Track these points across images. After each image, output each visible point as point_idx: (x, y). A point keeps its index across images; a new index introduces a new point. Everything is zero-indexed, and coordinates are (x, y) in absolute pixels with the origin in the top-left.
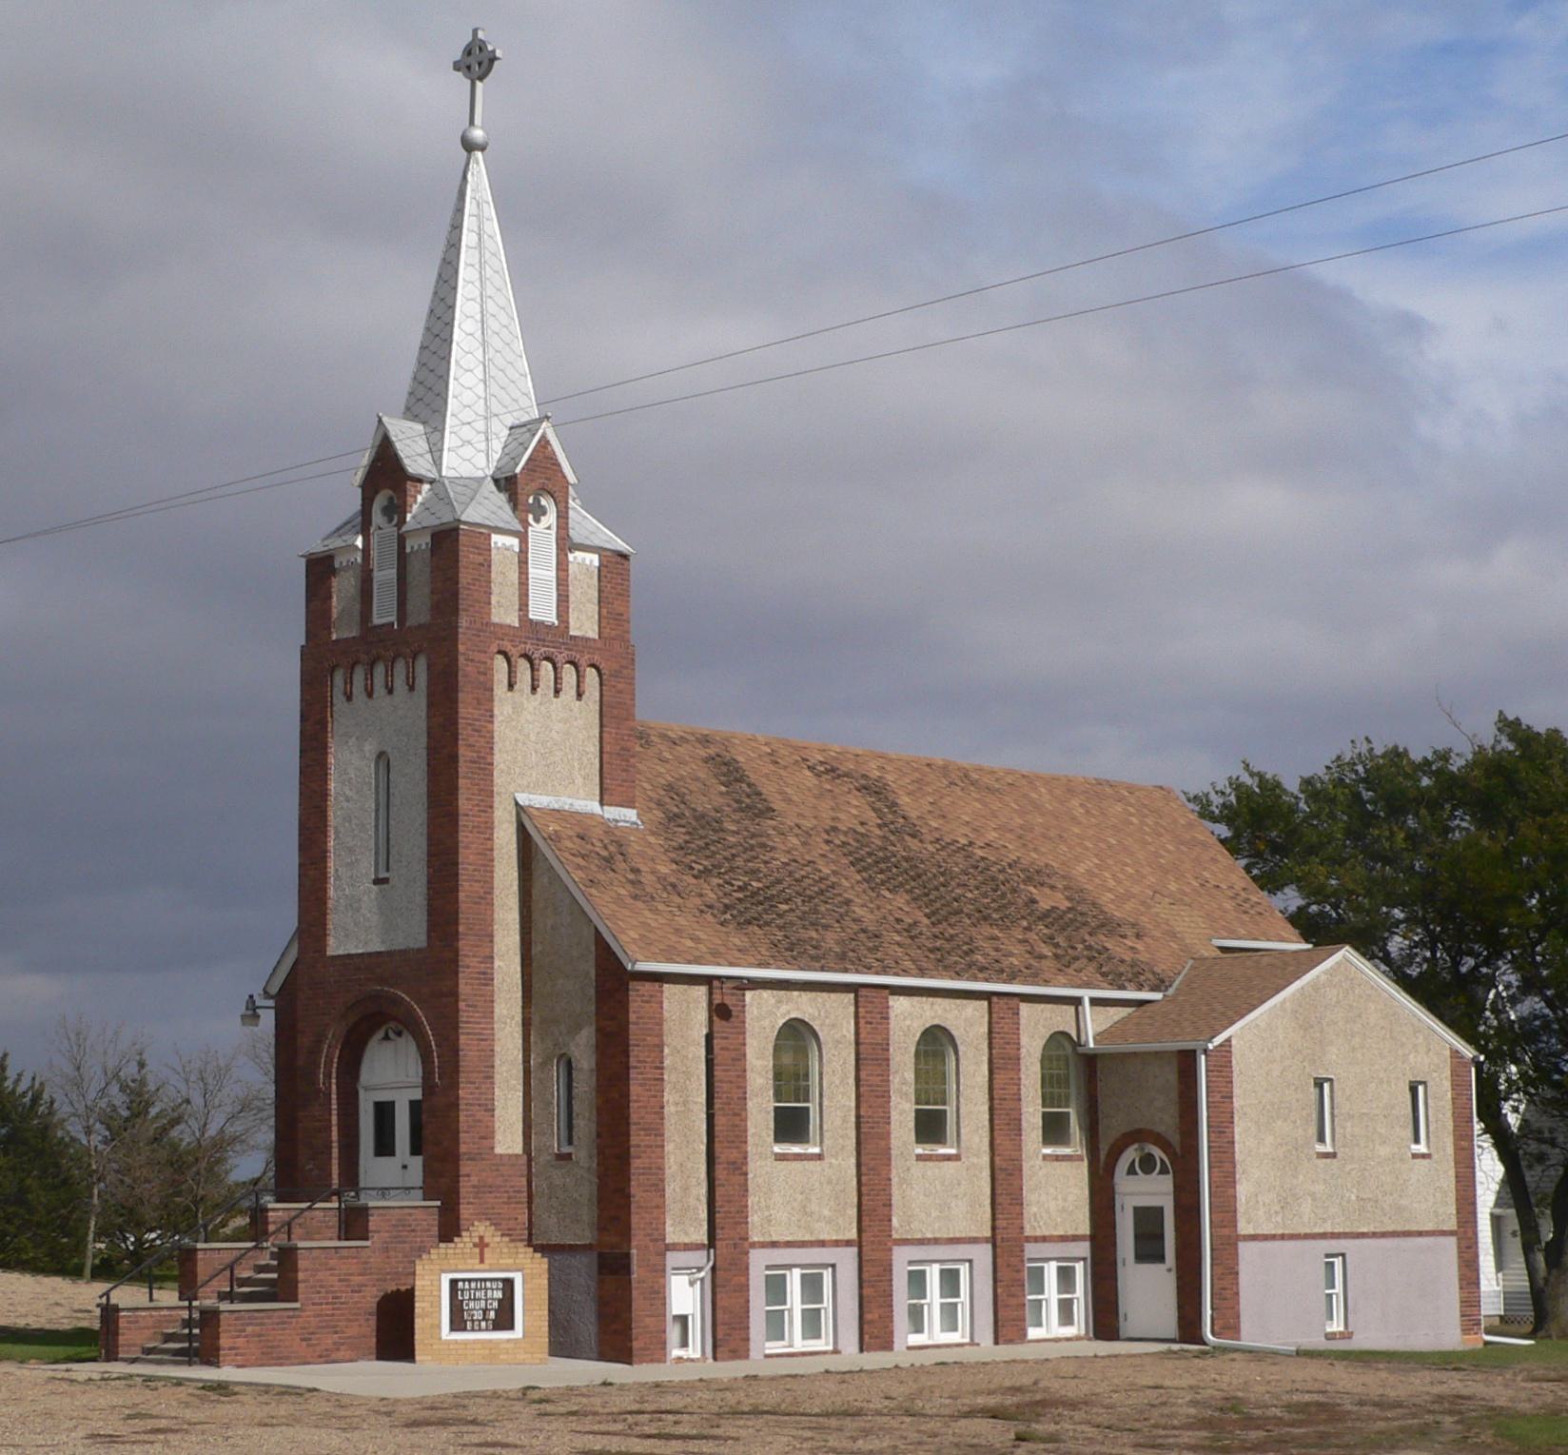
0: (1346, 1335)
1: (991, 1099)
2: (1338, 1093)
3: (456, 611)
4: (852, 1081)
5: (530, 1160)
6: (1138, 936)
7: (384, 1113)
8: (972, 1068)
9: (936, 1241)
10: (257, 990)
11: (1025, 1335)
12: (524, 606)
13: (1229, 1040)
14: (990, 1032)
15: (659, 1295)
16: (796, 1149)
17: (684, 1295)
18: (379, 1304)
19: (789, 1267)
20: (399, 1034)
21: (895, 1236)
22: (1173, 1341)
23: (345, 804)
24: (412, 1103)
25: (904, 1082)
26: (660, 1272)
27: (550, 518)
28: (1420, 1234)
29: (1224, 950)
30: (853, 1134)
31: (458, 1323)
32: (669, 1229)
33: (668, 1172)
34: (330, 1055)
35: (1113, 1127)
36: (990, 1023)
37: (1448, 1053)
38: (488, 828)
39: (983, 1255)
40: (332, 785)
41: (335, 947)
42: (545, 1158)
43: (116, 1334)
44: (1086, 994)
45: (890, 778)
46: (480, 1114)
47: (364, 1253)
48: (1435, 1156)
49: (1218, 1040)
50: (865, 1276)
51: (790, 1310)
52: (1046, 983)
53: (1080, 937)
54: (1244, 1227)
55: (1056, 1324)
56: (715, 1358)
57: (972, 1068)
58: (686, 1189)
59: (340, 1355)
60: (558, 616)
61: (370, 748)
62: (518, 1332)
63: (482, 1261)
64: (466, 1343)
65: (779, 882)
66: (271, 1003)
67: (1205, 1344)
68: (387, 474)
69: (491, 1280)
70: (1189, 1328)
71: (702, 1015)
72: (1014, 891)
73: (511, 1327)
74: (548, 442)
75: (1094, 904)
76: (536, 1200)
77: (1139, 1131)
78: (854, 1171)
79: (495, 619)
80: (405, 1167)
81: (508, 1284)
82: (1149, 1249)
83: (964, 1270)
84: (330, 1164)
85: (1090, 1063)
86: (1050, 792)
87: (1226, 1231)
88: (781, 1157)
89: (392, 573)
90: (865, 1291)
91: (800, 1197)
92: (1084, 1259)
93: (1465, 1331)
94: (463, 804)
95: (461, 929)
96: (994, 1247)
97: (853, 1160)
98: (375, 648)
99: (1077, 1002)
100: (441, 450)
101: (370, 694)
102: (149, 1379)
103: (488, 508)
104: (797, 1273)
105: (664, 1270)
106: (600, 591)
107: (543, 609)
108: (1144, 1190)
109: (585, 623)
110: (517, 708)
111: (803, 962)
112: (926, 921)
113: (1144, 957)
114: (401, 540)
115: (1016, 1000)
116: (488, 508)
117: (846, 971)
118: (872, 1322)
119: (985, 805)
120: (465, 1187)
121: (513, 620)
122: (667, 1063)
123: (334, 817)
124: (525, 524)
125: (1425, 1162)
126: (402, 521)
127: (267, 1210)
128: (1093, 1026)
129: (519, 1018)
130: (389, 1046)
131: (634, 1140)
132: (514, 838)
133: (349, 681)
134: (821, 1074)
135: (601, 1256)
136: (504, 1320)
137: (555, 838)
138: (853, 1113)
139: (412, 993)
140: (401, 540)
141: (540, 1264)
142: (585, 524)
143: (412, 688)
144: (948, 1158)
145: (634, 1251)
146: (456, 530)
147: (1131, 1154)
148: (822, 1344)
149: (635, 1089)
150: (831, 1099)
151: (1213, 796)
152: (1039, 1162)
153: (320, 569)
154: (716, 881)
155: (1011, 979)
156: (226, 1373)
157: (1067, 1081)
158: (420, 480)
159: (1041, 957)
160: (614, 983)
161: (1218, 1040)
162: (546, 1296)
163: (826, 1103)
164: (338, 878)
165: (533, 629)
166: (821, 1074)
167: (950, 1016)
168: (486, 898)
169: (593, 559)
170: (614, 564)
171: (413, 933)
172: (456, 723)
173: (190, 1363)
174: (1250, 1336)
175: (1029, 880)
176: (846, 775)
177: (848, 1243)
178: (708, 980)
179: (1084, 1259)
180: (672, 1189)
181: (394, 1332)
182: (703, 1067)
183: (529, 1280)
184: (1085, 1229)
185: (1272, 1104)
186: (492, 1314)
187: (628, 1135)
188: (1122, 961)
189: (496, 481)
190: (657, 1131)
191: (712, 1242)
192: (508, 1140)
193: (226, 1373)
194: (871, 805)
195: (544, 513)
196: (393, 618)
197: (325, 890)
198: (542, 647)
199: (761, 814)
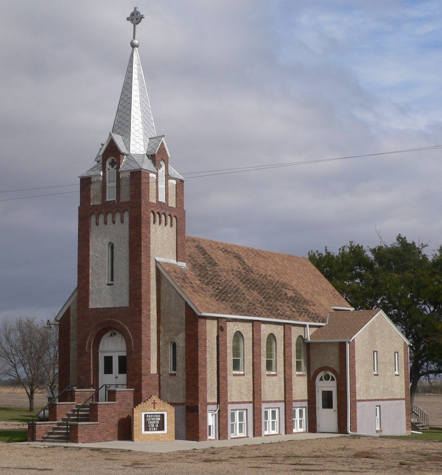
0: (381, 431)
1: (284, 356)
2: (378, 356)
3: (140, 197)
4: (251, 351)
5: (160, 375)
6: (314, 305)
7: (108, 361)
8: (280, 347)
9: (271, 402)
10: (52, 320)
11: (293, 431)
12: (157, 197)
13: (354, 339)
14: (284, 335)
15: (205, 419)
16: (237, 373)
17: (211, 420)
18: (119, 422)
19: (236, 410)
20: (115, 334)
21: (262, 400)
22: (336, 433)
23: (96, 259)
24: (120, 358)
25: (264, 352)
26: (205, 412)
27: (163, 168)
28: (397, 399)
29: (334, 310)
30: (251, 367)
31: (147, 429)
32: (208, 398)
33: (207, 380)
34: (91, 339)
35: (316, 365)
36: (284, 332)
37: (403, 343)
38: (149, 268)
39: (282, 405)
40: (91, 253)
41: (92, 305)
42: (166, 375)
43: (35, 432)
44: (308, 324)
45: (240, 253)
46: (147, 361)
47: (115, 406)
48: (400, 375)
49: (352, 339)
50: (255, 412)
51: (236, 424)
52: (298, 320)
53: (300, 306)
54: (358, 398)
55: (300, 427)
56: (219, 439)
57: (280, 347)
58: (212, 385)
59: (108, 439)
60: (166, 200)
61: (107, 241)
62: (165, 431)
63: (154, 408)
64: (149, 435)
65: (226, 287)
66: (57, 323)
67: (348, 434)
68: (112, 153)
69: (157, 414)
70: (342, 428)
71: (215, 330)
72: (281, 291)
73: (163, 429)
74: (163, 144)
75: (300, 295)
76: (162, 389)
77: (325, 367)
78: (252, 379)
79: (150, 201)
80: (117, 377)
81: (162, 416)
82: (327, 404)
83: (277, 410)
84: (90, 376)
85: (308, 345)
86: (279, 258)
87: (354, 399)
88: (235, 375)
89: (114, 184)
90: (256, 418)
91: (239, 388)
92: (306, 407)
94: (143, 261)
95: (142, 301)
96: (285, 403)
97: (252, 376)
98: (108, 208)
99: (305, 326)
100: (129, 145)
101: (106, 223)
102: (65, 447)
103: (147, 165)
104: (238, 411)
105: (206, 411)
106: (176, 192)
107: (162, 199)
108: (325, 385)
109: (172, 203)
110: (156, 230)
111: (240, 313)
112: (264, 300)
113: (317, 312)
114: (118, 174)
115: (290, 325)
116: (147, 165)
117: (251, 316)
118: (257, 427)
119: (265, 262)
120: (143, 384)
121: (154, 201)
122: (207, 345)
123: (92, 263)
124: (158, 171)
126: (118, 168)
127: (75, 391)
128: (309, 333)
129: (156, 330)
131: (199, 369)
132: (155, 272)
133: (97, 219)
134: (244, 349)
135: (187, 407)
136: (161, 427)
137: (168, 272)
138: (252, 361)
139: (126, 321)
140: (118, 174)
141: (172, 409)
142: (173, 171)
143: (122, 222)
144: (274, 375)
145: (199, 405)
146: (141, 171)
147: (322, 374)
148: (243, 435)
149: (200, 353)
150: (372, 362)
151: (316, 255)
152: (295, 376)
153: (86, 182)
154: (211, 286)
155: (289, 319)
156: (80, 445)
157: (301, 350)
158: (123, 155)
159: (294, 312)
160: (193, 320)
161: (352, 339)
162: (174, 420)
163: (245, 358)
164: (93, 283)
166: (244, 349)
167: (275, 330)
168: (148, 291)
169: (174, 182)
170: (180, 183)
171: (123, 301)
172: (141, 234)
173: (67, 442)
174: (360, 431)
175: (283, 287)
176: (230, 252)
177: (250, 402)
178: (217, 319)
179: (306, 407)
180: (209, 385)
181: (126, 431)
182: (216, 346)
183: (169, 414)
184: (306, 397)
185: (364, 359)
186: (157, 425)
187: (198, 368)
188: (313, 313)
189: (148, 156)
190: (205, 367)
191: (218, 403)
192: (154, 370)
193: (80, 445)
194: (239, 262)
195: (161, 167)
196: (115, 199)
197: (88, 287)
198: (162, 211)
199: (214, 265)
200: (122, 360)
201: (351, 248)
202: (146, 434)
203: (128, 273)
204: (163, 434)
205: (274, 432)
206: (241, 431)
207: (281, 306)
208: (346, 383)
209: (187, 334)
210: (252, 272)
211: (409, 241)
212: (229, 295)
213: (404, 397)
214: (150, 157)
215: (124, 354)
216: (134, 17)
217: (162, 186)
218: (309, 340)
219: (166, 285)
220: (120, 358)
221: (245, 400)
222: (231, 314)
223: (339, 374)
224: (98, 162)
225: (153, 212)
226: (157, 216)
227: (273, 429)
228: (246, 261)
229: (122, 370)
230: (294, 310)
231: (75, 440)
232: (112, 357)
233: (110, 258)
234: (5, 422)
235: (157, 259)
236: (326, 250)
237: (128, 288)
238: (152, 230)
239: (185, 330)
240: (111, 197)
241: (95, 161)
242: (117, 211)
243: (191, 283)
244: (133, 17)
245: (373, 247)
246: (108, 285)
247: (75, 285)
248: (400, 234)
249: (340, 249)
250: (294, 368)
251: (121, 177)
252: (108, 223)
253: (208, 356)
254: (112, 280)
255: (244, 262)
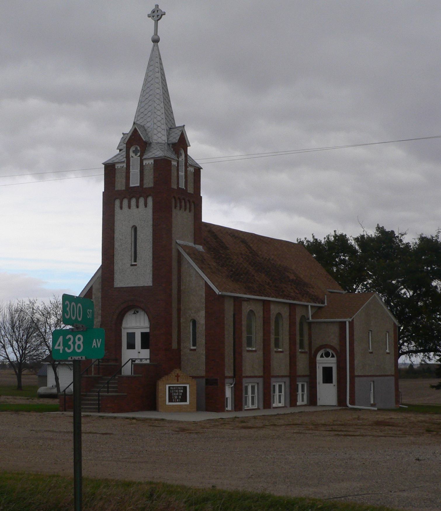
7: (131, 336)
12: (178, 184)
17: (228, 393)
20: (138, 312)
24: (143, 334)
28: (388, 376)
29: (329, 292)
31: (170, 400)
44: (310, 304)
52: (301, 301)
54: (356, 374)
60: (185, 186)
62: (188, 403)
63: (178, 381)
64: (173, 406)
77: (326, 345)
80: (139, 352)
81: (185, 388)
82: (328, 379)
88: (248, 351)
93: (396, 404)
99: (307, 306)
107: (182, 186)
109: (191, 190)
117: (262, 296)
121: (175, 187)
123: (117, 245)
125: (281, 354)
130: (134, 316)
133: (137, 202)
135: (206, 380)
136: (184, 399)
143: (146, 206)
151: (305, 242)
152: (189, 351)
165: (183, 192)
180: (226, 360)
200: (144, 335)
201: (335, 236)
202: (170, 405)
203: (151, 255)
204: (185, 405)
205: (280, 405)
206: (253, 403)
207: (286, 288)
208: (346, 360)
209: (206, 312)
210: (258, 256)
211: (388, 229)
212: (242, 277)
213: (393, 374)
214: (171, 145)
215: (148, 330)
216: (155, 14)
217: (182, 174)
218: (310, 319)
219: (186, 266)
220: (143, 334)
221: (256, 375)
222: (245, 294)
223: (339, 351)
224: (120, 150)
225: (174, 197)
226: (178, 201)
227: (280, 402)
228: (251, 245)
229: (144, 346)
230: (297, 291)
231: (152, 404)
232: (134, 333)
233: (133, 240)
234: (6, 397)
235: (178, 241)
236: (313, 237)
237: (151, 269)
238: (174, 215)
239: (204, 308)
240: (135, 182)
241: (118, 149)
242: (141, 196)
243: (209, 264)
244: (153, 14)
245: (356, 237)
246: (132, 265)
247: (101, 264)
248: (378, 225)
249: (325, 238)
250: (298, 346)
251: (144, 164)
252: (132, 208)
253: (226, 333)
254: (135, 261)
255: (250, 247)
